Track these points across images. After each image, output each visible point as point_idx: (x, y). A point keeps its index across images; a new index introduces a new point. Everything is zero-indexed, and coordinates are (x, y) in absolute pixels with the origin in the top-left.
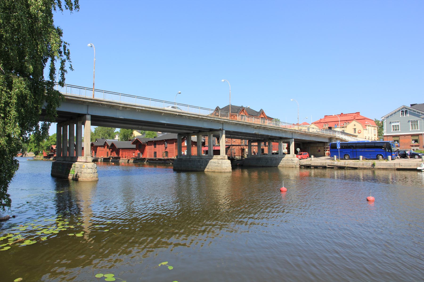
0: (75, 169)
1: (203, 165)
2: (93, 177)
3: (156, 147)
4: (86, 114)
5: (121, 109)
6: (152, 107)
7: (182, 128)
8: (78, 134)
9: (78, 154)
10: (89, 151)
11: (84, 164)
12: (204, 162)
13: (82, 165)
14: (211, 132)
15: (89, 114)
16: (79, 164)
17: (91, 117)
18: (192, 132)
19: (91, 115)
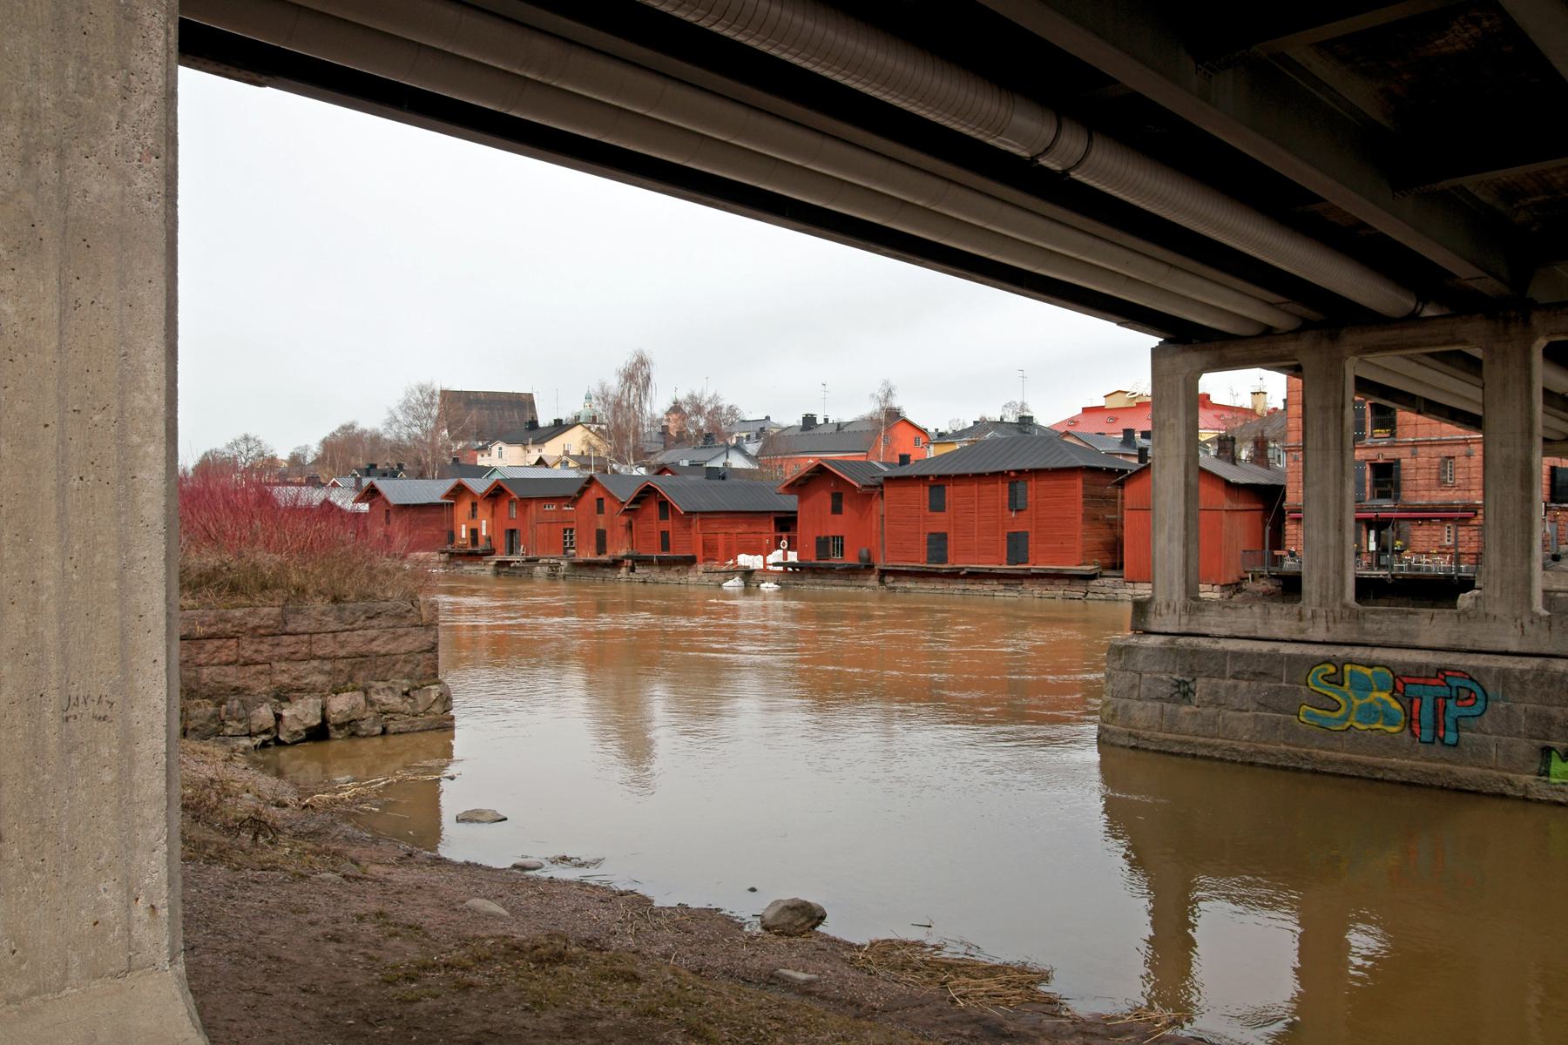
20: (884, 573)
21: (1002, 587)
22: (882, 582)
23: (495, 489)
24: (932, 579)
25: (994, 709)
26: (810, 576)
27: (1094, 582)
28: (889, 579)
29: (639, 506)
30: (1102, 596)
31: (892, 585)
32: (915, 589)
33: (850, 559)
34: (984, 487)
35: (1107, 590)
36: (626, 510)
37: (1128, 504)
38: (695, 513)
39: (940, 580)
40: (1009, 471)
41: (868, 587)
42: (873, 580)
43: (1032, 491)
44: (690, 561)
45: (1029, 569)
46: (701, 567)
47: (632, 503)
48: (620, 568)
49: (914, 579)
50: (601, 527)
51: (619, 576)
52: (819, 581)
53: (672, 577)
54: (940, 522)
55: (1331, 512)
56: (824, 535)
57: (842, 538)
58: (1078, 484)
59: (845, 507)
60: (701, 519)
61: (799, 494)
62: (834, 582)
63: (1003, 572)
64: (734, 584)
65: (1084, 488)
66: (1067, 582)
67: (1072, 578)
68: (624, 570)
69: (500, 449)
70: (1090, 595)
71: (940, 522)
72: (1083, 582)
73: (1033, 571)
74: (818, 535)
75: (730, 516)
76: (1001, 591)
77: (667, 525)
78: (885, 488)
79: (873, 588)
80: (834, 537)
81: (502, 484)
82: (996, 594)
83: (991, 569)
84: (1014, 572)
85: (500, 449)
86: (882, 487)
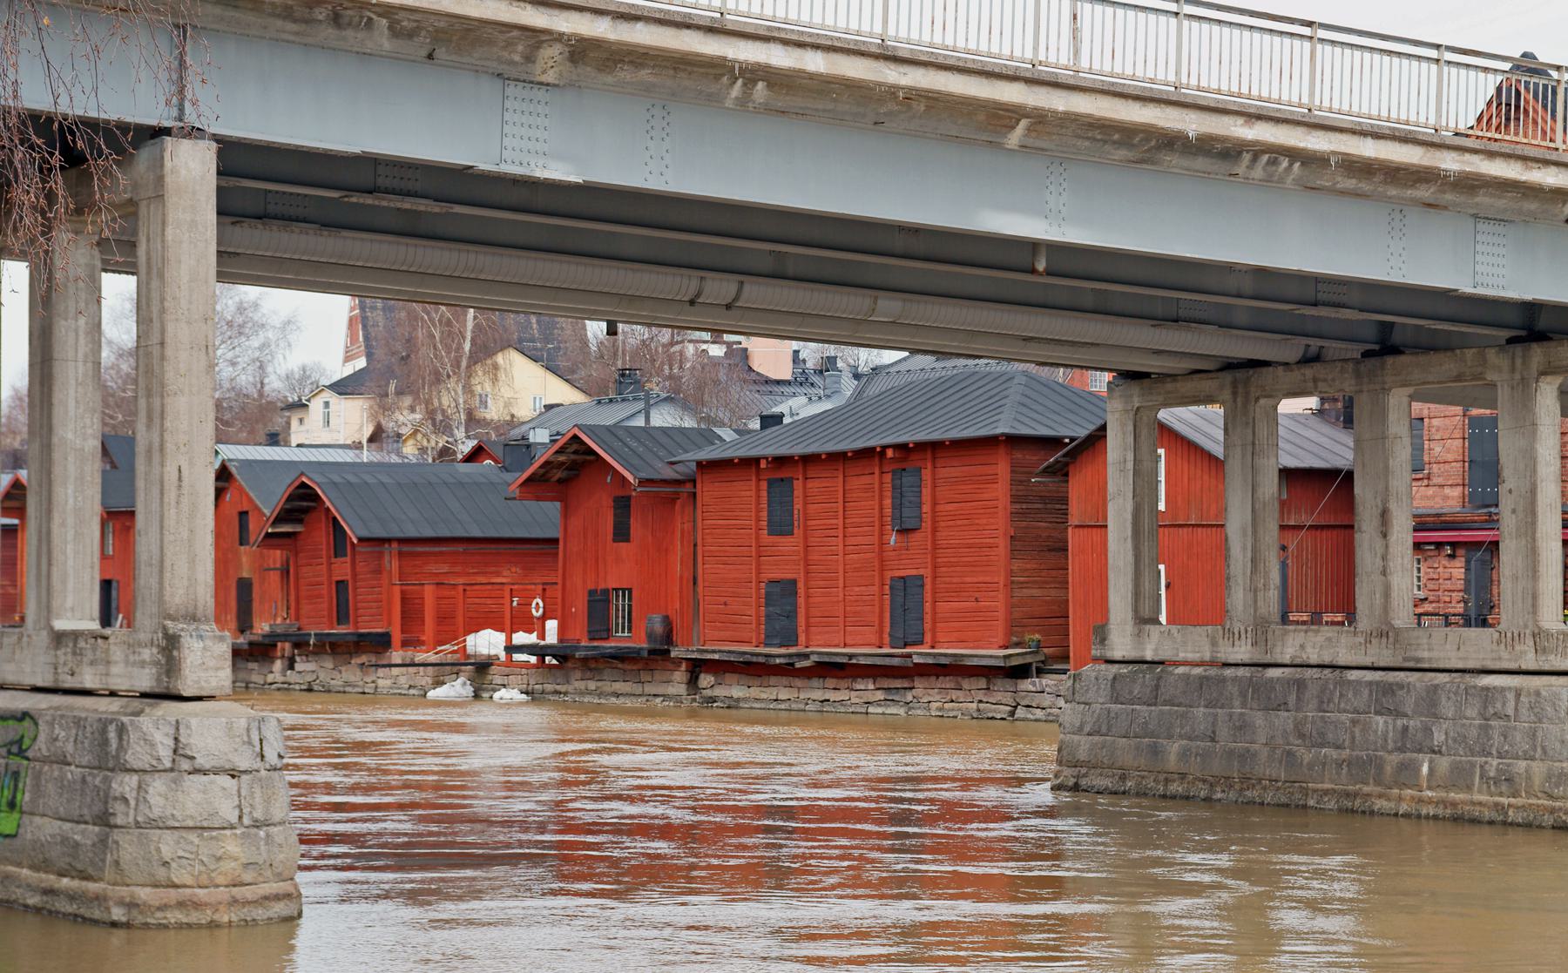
0: (27, 781)
1: (1438, 737)
2: (248, 877)
3: (592, 593)
4: (167, 132)
5: (550, 77)
6: (908, 31)
7: (44, 530)
8: (58, 368)
9: (56, 603)
10: (192, 562)
11: (145, 722)
12: (1447, 708)
13: (122, 730)
14: (1537, 353)
15: (195, 133)
16: (78, 722)
17: (220, 154)
18: (1290, 350)
19: (217, 139)
20: (697, 667)
21: (880, 695)
22: (693, 682)
23: (290, 499)
24: (773, 680)
25: (981, 939)
26: (578, 674)
27: (1026, 685)
28: (706, 680)
29: (299, 528)
30: (1039, 714)
31: (708, 693)
32: (745, 699)
33: (634, 639)
34: (856, 483)
35: (1047, 700)
36: (268, 535)
37: (1074, 520)
38: (389, 540)
39: (785, 680)
40: (884, 448)
41: (665, 697)
42: (677, 684)
43: (809, 492)
44: (380, 643)
45: (909, 656)
46: (397, 656)
47: (278, 520)
48: (272, 660)
49: (745, 679)
50: (245, 575)
51: (270, 678)
52: (592, 685)
53: (352, 678)
54: (784, 558)
55: (427, 549)
56: (602, 586)
57: (630, 590)
58: (1001, 466)
59: (636, 527)
60: (400, 554)
61: (563, 499)
62: (619, 686)
63: (869, 661)
64: (457, 688)
65: (1013, 482)
66: (982, 683)
67: (989, 673)
68: (278, 665)
69: (327, 404)
70: (1020, 713)
71: (784, 558)
72: (1008, 684)
73: (916, 660)
74: (591, 586)
75: (472, 548)
76: (878, 703)
77: (342, 569)
78: (699, 486)
79: (677, 698)
80: (617, 590)
81: (315, 482)
82: (871, 710)
83: (851, 656)
84: (878, 661)
85: (327, 404)
86: (694, 482)
